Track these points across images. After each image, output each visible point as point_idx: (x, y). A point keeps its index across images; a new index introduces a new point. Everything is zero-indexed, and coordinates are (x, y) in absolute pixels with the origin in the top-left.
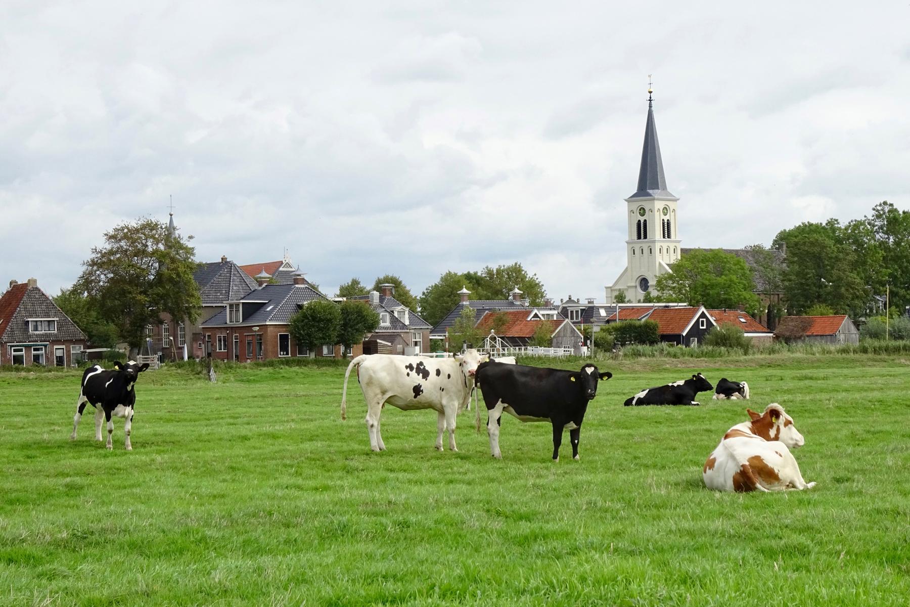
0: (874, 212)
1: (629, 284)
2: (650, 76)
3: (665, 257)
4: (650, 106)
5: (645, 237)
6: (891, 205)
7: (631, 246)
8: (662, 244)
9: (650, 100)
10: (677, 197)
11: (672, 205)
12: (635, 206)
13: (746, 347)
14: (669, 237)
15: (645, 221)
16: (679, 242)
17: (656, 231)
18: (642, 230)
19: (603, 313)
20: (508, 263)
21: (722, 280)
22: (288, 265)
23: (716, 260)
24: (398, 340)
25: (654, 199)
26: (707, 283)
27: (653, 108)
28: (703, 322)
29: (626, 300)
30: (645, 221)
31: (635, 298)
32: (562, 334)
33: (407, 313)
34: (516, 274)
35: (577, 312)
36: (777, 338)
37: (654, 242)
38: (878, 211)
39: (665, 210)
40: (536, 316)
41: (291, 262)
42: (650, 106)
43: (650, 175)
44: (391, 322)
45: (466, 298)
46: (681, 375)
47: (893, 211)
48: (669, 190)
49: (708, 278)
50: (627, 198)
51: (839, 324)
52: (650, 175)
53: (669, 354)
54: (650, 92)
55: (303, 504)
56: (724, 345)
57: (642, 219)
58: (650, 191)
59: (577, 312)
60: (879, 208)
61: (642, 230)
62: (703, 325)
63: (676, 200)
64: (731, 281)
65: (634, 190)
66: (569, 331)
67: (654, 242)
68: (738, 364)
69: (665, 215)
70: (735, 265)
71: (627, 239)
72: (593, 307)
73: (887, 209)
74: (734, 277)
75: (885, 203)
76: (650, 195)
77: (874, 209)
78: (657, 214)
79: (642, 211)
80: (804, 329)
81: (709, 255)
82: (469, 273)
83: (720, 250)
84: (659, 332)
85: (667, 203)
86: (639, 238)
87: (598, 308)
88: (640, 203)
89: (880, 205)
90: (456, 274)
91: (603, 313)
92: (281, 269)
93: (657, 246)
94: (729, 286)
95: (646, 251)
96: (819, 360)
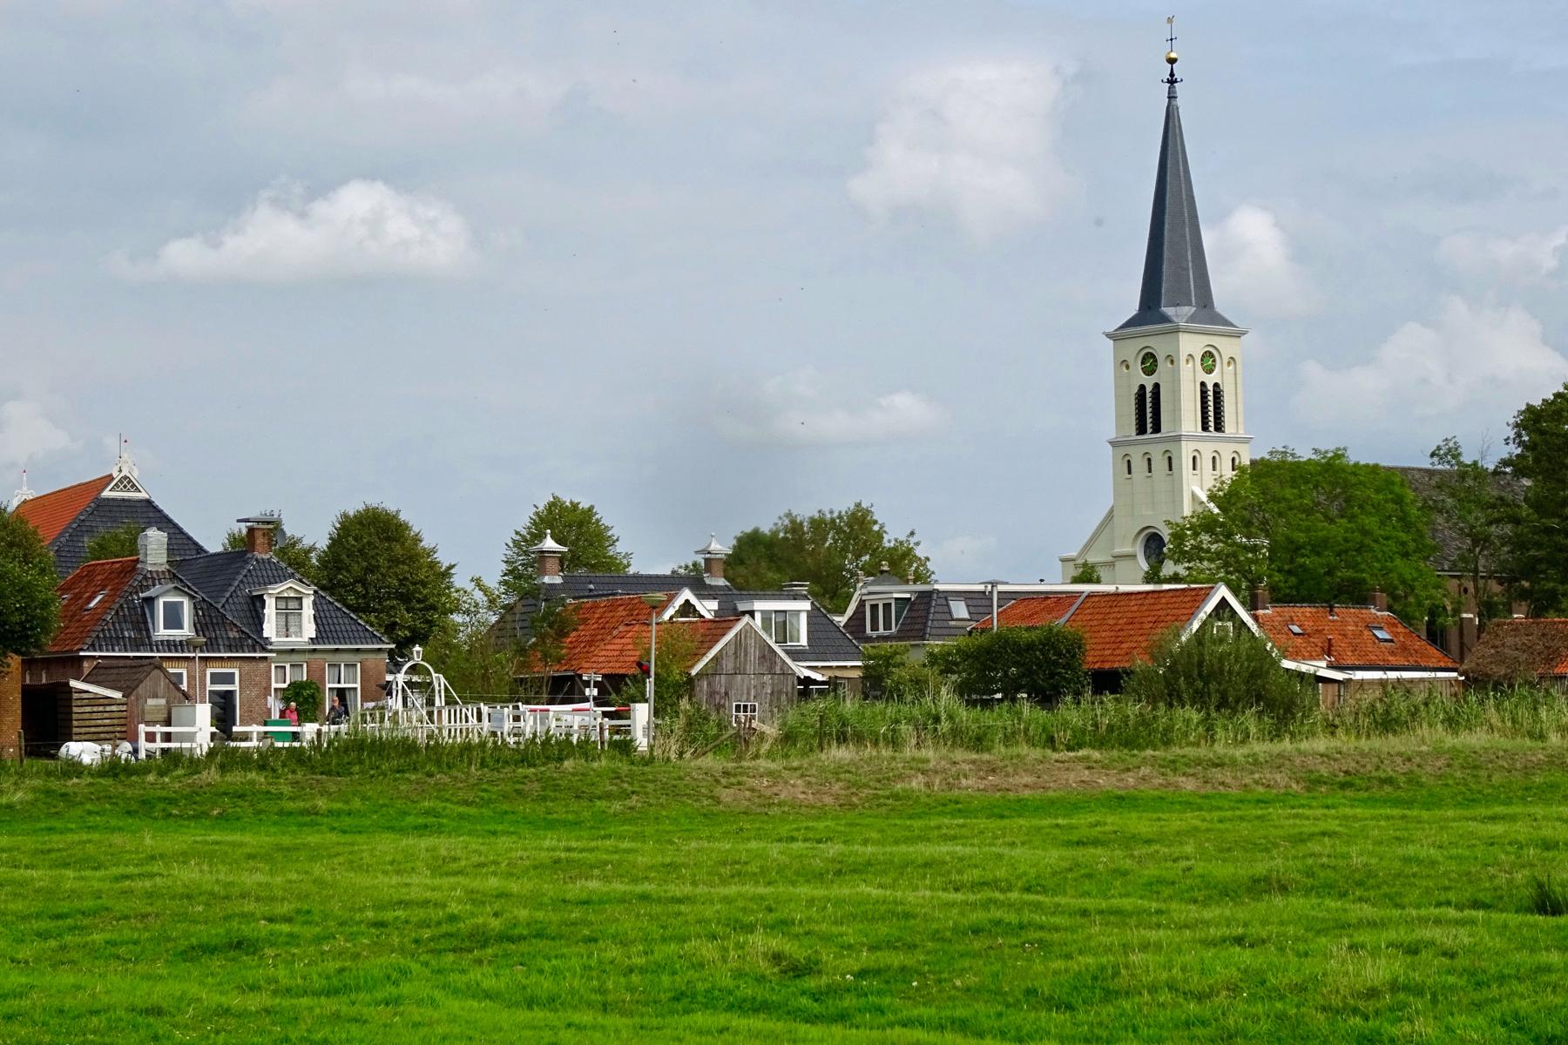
1: (1118, 550)
2: (1170, 20)
3: (1199, 482)
4: (1172, 97)
5: (1157, 429)
7: (1124, 450)
9: (1172, 81)
10: (1241, 326)
11: (1227, 347)
12: (1132, 350)
13: (1282, 704)
15: (1157, 386)
16: (1246, 441)
17: (1185, 414)
18: (1148, 411)
19: (960, 610)
20: (838, 504)
21: (1338, 530)
22: (126, 482)
23: (1332, 477)
24: (154, 680)
25: (1177, 331)
26: (1301, 537)
27: (1179, 102)
30: (1157, 386)
31: (876, 528)
32: (728, 665)
33: (308, 603)
34: (858, 529)
35: (887, 606)
36: (1475, 682)
37: (1178, 439)
39: (1208, 360)
40: (687, 608)
41: (135, 475)
42: (1172, 97)
43: (1172, 273)
44: (199, 626)
45: (552, 564)
48: (1220, 302)
49: (1314, 533)
50: (1111, 329)
52: (1172, 273)
53: (957, 736)
54: (1172, 61)
55: (1305, 830)
56: (1199, 699)
57: (1210, 381)
58: (1169, 311)
59: (887, 606)
61: (1148, 411)
63: (1238, 335)
64: (1365, 533)
65: (1133, 308)
66: (754, 654)
67: (1178, 439)
68: (1217, 774)
69: (1210, 371)
70: (1378, 491)
71: (1112, 434)
72: (926, 596)
74: (1371, 522)
76: (1165, 319)
79: (1150, 362)
84: (1092, 659)
86: (1141, 430)
87: (947, 595)
90: (575, 506)
91: (960, 610)
92: (106, 493)
93: (1187, 450)
95: (1159, 464)
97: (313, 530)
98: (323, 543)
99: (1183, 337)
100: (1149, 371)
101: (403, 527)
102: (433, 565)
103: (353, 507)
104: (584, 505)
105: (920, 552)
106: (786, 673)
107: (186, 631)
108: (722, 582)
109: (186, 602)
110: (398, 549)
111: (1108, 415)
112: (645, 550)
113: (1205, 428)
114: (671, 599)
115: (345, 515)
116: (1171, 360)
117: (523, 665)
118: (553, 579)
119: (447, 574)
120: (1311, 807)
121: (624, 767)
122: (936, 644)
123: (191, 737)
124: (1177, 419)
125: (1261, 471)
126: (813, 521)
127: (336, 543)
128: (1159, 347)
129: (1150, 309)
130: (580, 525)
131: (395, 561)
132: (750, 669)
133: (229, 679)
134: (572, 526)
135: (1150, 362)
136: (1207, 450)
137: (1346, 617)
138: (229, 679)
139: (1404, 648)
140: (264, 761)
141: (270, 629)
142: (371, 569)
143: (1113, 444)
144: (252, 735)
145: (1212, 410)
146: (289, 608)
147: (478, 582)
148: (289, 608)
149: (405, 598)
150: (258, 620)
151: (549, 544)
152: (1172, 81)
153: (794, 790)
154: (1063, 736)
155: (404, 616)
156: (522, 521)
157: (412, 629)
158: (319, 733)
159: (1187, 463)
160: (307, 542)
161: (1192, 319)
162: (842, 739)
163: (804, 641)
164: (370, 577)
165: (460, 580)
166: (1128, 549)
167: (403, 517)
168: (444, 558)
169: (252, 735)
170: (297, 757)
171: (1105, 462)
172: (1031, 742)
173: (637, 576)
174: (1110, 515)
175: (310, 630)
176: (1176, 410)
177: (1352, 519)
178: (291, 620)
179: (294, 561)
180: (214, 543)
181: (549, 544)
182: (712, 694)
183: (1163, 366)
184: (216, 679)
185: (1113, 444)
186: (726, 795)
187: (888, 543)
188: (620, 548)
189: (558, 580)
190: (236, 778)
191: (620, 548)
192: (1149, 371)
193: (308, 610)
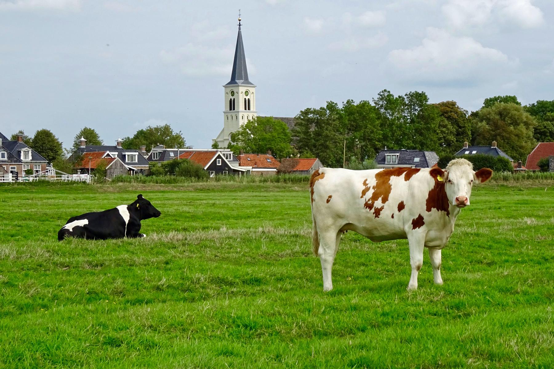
0: (378, 96)
1: (225, 138)
4: (240, 29)
5: (234, 109)
6: (389, 92)
8: (244, 113)
11: (251, 90)
14: (249, 109)
17: (241, 106)
18: (232, 105)
25: (239, 86)
28: (219, 161)
29: (220, 147)
32: (114, 167)
33: (30, 152)
37: (238, 112)
38: (381, 95)
39: (247, 93)
40: (108, 155)
42: (240, 29)
43: (239, 73)
44: (8, 158)
46: (125, 196)
47: (390, 95)
48: (250, 80)
51: (312, 164)
52: (239, 73)
54: (240, 20)
57: (247, 98)
58: (237, 81)
60: (382, 94)
61: (232, 105)
62: (219, 163)
66: (119, 165)
69: (247, 96)
71: (224, 110)
73: (386, 94)
75: (385, 91)
76: (236, 83)
77: (379, 94)
78: (241, 95)
79: (233, 93)
80: (293, 167)
81: (264, 121)
82: (142, 130)
83: (271, 118)
85: (249, 88)
86: (231, 109)
88: (231, 88)
89: (382, 92)
90: (90, 129)
94: (273, 139)
95: (234, 118)
96: (258, 187)
97: (31, 135)
98: (33, 137)
99: (240, 88)
100: (233, 95)
101: (51, 134)
102: (58, 142)
103: (40, 129)
104: (92, 129)
105: (182, 136)
106: (125, 168)
107: (6, 159)
108: (121, 147)
109: (6, 153)
110: (50, 139)
111: (223, 106)
112: (109, 137)
113: (245, 109)
114: (105, 153)
115: (38, 131)
116: (237, 93)
117: (74, 166)
118: (83, 147)
119: (61, 144)
120: (174, 192)
121: (84, 186)
122: (165, 162)
123: (8, 180)
124: (238, 108)
125: (260, 120)
126: (155, 128)
127: (36, 137)
128: (235, 90)
129: (233, 81)
130: (91, 133)
131: (49, 142)
132: (118, 168)
133: (14, 168)
134: (89, 135)
135: (233, 93)
136: (246, 115)
137: (261, 157)
138: (14, 168)
139: (274, 163)
140: (24, 184)
141: (22, 158)
142: (45, 143)
143: (224, 112)
144: (20, 180)
145: (247, 105)
146: (26, 153)
147: (65, 149)
148: (26, 153)
149: (51, 150)
150: (20, 156)
151: (83, 139)
152: (240, 25)
153: (111, 189)
154: (159, 181)
155: (51, 154)
156: (78, 132)
157: (53, 157)
158: (438, 117)
159: (240, 118)
160: (29, 137)
161: (243, 83)
162: (122, 181)
163: (137, 161)
164: (44, 145)
165: (64, 146)
166: (227, 138)
167: (51, 132)
168: (60, 141)
169: (20, 180)
170: (30, 183)
171: (222, 117)
172: (153, 182)
173: (103, 146)
174: (223, 130)
175: (30, 158)
176: (238, 105)
177: (271, 132)
178: (27, 155)
179: (27, 142)
180: (9, 138)
181: (83, 139)
182: (110, 173)
183: (235, 94)
184: (12, 168)
185: (224, 112)
186: (99, 190)
187: (174, 134)
188: (100, 139)
189: (84, 147)
190: (20, 186)
191: (100, 139)
192: (233, 95)
193: (30, 154)
